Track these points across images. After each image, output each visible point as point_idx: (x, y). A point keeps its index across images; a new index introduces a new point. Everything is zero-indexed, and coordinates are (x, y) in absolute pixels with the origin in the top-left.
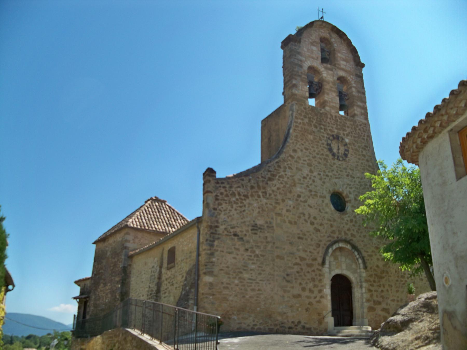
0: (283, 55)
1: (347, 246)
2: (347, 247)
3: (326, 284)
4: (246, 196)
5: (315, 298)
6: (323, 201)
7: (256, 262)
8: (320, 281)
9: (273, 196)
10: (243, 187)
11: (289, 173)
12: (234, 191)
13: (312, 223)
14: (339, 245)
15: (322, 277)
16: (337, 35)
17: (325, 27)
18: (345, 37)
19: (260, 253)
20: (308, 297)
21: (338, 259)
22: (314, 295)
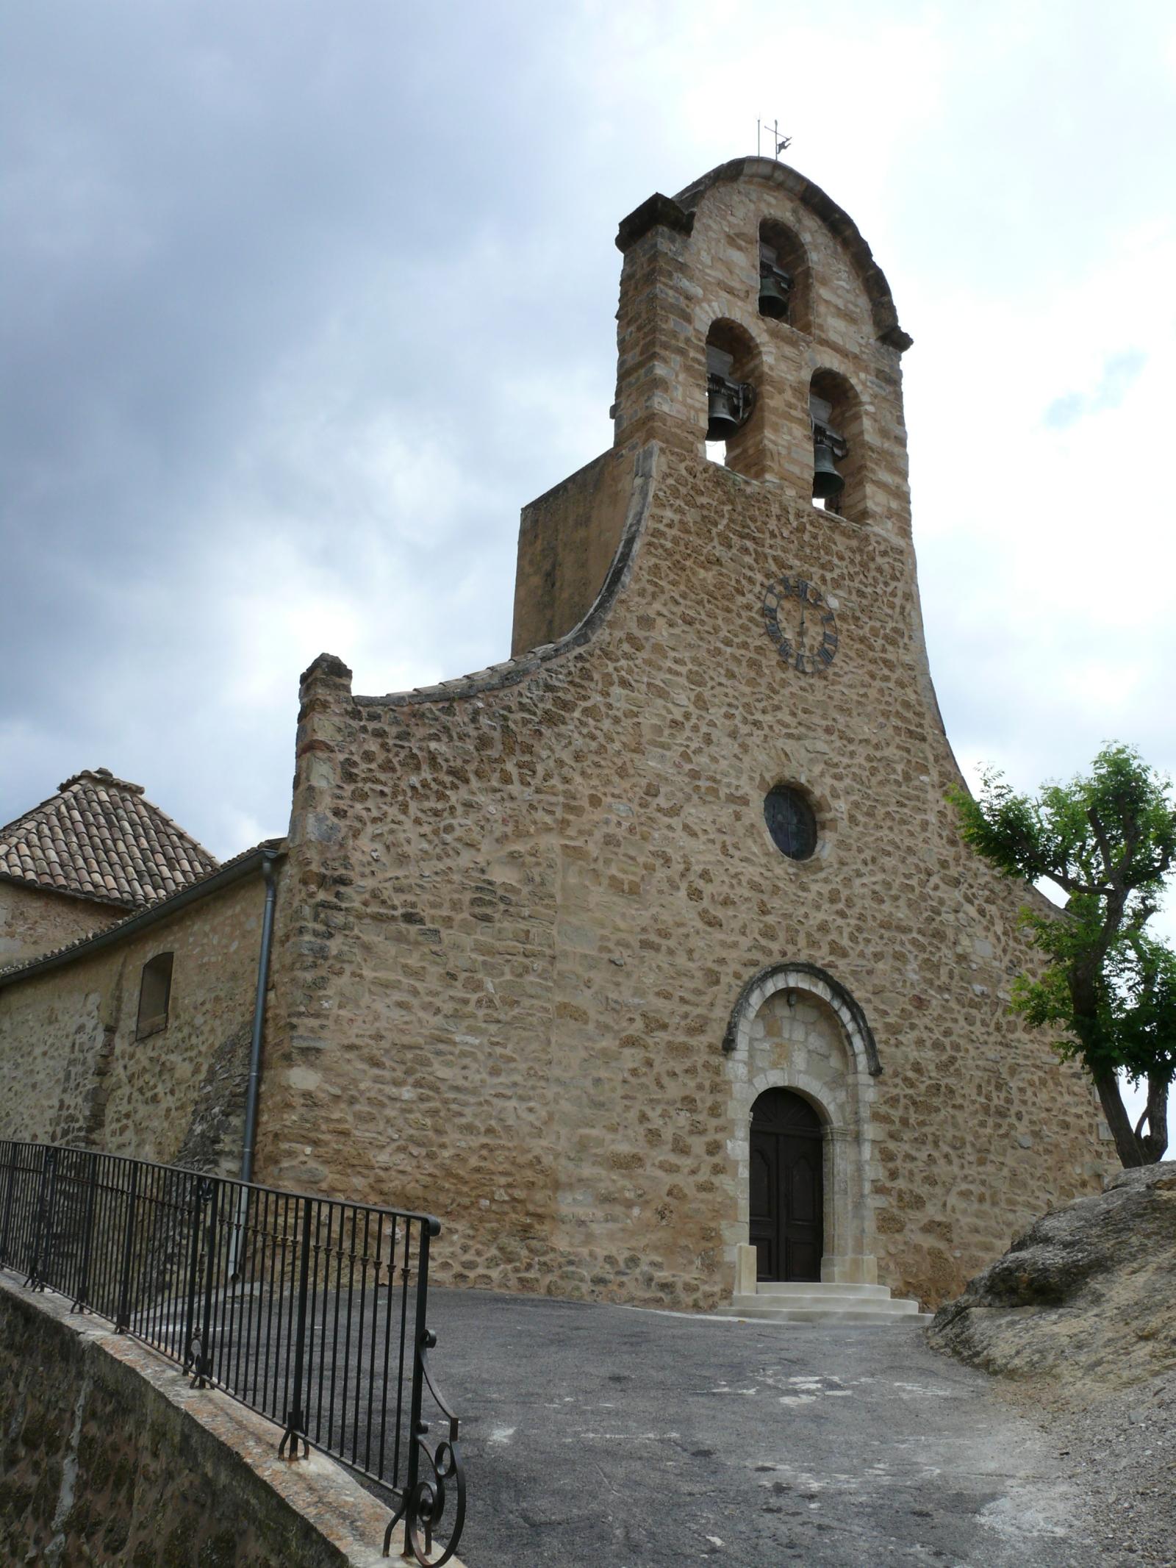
1: (816, 986)
2: (814, 990)
8: (715, 1111)
13: (695, 894)
15: (719, 1098)
21: (779, 1034)
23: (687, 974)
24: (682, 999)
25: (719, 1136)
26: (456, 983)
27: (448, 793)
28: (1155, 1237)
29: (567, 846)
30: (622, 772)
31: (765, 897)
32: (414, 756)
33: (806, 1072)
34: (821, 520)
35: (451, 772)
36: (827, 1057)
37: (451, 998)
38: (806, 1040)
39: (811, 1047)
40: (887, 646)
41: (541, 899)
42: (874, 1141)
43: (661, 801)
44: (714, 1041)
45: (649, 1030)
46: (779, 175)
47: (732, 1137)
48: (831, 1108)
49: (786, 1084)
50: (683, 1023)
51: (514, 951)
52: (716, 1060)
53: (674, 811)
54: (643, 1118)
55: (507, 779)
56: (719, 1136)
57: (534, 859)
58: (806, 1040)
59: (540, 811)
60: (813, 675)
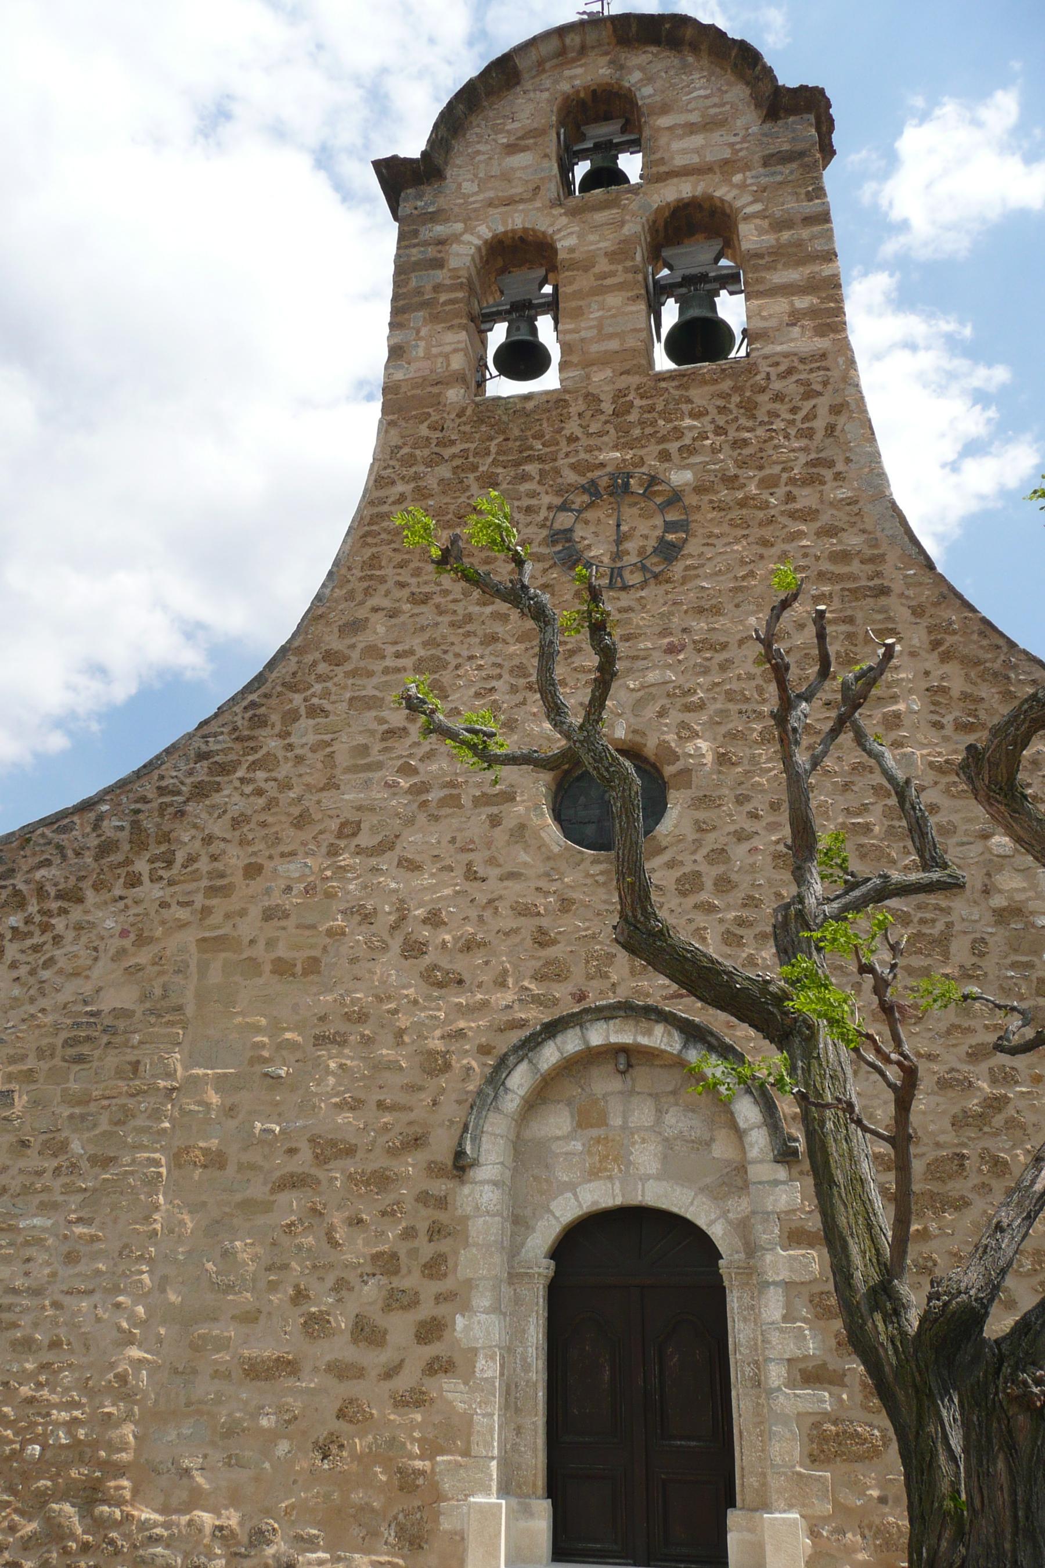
0: (398, 256)
1: (649, 1033)
2: (643, 1040)
3: (469, 1284)
4: (72, 896)
5: (390, 1373)
6: (495, 821)
7: (60, 1198)
8: (435, 1268)
9: (203, 865)
10: (64, 857)
11: (305, 732)
12: (21, 886)
13: (414, 949)
14: (584, 1039)
15: (444, 1246)
16: (654, 49)
17: (583, 50)
18: (689, 33)
19: (92, 1150)
20: (341, 1371)
21: (602, 1121)
22: (383, 1357)
23: (393, 1067)
24: (380, 1105)
25: (442, 1310)
26: (29, 1152)
27: (53, 921)
28: (758, 221)
29: (204, 940)
30: (301, 821)
31: (545, 922)
32: (17, 893)
33: (658, 1178)
34: (663, 384)
35: (60, 896)
36: (708, 1143)
37: (21, 1171)
38: (659, 1121)
39: (668, 1133)
40: (796, 491)
41: (160, 1016)
42: (787, 1285)
43: (365, 839)
44: (439, 1158)
45: (321, 1160)
46: (573, 40)
47: (466, 1308)
48: (717, 1232)
49: (619, 1201)
50: (382, 1140)
51: (114, 1093)
52: (440, 1187)
53: (385, 847)
54: (300, 1296)
55: (134, 881)
56: (442, 1310)
57: (157, 968)
58: (659, 1121)
59: (174, 907)
60: (644, 585)
